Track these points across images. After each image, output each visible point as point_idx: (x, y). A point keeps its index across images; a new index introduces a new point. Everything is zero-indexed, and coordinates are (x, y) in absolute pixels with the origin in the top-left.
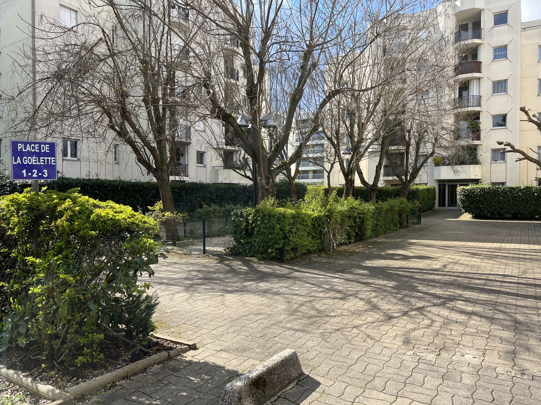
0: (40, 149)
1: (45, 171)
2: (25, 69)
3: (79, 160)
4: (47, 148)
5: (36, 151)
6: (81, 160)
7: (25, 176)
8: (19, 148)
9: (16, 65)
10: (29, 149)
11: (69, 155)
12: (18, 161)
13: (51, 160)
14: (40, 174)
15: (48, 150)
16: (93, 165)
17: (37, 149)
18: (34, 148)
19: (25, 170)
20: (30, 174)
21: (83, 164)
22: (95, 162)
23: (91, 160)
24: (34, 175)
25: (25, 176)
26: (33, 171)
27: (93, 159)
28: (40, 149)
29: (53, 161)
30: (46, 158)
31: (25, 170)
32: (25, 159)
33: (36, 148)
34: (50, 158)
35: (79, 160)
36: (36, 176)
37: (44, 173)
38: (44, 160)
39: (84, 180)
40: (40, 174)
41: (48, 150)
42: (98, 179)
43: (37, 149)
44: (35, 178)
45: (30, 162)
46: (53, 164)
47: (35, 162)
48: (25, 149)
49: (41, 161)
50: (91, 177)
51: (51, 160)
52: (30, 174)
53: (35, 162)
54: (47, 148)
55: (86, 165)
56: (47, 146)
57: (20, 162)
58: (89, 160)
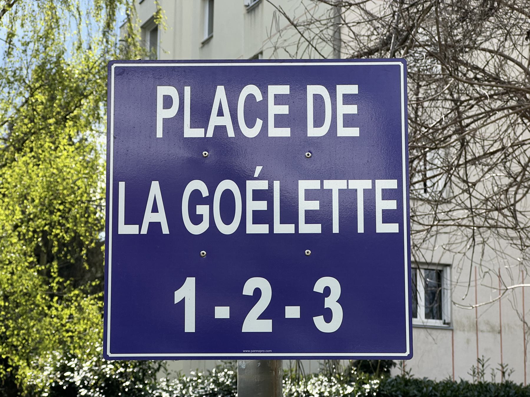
0: (295, 120)
1: (329, 285)
2: (306, 35)
3: (448, 326)
4: (344, 109)
5: (274, 132)
6: (455, 325)
7: (190, 326)
8: (163, 114)
9: (284, 22)
10: (226, 121)
11: (421, 310)
12: (149, 217)
13: (369, 195)
14: (293, 312)
15: (349, 121)
16: (488, 340)
17: (280, 121)
18: (256, 111)
19: (190, 283)
20: (222, 312)
21: (460, 336)
22: (492, 330)
23: (481, 327)
24: (254, 323)
25: (190, 326)
26: (248, 289)
27: (488, 323)
28: (295, 120)
29: (382, 205)
30: (335, 186)
31: (190, 283)
32: (196, 193)
33: (274, 109)
34: (360, 185)
35: (448, 326)
36: (267, 326)
37: (315, 305)
38: (324, 196)
39: (466, 385)
40: (293, 312)
41: (349, 121)
42: (508, 385)
43: (280, 121)
44: (256, 341)
45: (228, 219)
46: (382, 228)
47: (260, 217)
48: (201, 117)
49: (305, 206)
50: (487, 378)
51: (369, 195)
52: (222, 312)
53: (260, 217)
54: (344, 109)
55: (468, 341)
56: (342, 90)
57: (161, 217)
58: (476, 328)
